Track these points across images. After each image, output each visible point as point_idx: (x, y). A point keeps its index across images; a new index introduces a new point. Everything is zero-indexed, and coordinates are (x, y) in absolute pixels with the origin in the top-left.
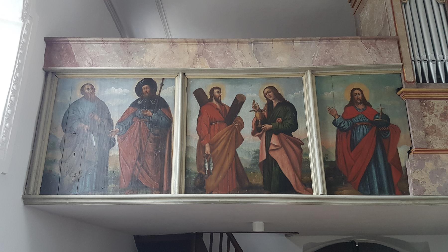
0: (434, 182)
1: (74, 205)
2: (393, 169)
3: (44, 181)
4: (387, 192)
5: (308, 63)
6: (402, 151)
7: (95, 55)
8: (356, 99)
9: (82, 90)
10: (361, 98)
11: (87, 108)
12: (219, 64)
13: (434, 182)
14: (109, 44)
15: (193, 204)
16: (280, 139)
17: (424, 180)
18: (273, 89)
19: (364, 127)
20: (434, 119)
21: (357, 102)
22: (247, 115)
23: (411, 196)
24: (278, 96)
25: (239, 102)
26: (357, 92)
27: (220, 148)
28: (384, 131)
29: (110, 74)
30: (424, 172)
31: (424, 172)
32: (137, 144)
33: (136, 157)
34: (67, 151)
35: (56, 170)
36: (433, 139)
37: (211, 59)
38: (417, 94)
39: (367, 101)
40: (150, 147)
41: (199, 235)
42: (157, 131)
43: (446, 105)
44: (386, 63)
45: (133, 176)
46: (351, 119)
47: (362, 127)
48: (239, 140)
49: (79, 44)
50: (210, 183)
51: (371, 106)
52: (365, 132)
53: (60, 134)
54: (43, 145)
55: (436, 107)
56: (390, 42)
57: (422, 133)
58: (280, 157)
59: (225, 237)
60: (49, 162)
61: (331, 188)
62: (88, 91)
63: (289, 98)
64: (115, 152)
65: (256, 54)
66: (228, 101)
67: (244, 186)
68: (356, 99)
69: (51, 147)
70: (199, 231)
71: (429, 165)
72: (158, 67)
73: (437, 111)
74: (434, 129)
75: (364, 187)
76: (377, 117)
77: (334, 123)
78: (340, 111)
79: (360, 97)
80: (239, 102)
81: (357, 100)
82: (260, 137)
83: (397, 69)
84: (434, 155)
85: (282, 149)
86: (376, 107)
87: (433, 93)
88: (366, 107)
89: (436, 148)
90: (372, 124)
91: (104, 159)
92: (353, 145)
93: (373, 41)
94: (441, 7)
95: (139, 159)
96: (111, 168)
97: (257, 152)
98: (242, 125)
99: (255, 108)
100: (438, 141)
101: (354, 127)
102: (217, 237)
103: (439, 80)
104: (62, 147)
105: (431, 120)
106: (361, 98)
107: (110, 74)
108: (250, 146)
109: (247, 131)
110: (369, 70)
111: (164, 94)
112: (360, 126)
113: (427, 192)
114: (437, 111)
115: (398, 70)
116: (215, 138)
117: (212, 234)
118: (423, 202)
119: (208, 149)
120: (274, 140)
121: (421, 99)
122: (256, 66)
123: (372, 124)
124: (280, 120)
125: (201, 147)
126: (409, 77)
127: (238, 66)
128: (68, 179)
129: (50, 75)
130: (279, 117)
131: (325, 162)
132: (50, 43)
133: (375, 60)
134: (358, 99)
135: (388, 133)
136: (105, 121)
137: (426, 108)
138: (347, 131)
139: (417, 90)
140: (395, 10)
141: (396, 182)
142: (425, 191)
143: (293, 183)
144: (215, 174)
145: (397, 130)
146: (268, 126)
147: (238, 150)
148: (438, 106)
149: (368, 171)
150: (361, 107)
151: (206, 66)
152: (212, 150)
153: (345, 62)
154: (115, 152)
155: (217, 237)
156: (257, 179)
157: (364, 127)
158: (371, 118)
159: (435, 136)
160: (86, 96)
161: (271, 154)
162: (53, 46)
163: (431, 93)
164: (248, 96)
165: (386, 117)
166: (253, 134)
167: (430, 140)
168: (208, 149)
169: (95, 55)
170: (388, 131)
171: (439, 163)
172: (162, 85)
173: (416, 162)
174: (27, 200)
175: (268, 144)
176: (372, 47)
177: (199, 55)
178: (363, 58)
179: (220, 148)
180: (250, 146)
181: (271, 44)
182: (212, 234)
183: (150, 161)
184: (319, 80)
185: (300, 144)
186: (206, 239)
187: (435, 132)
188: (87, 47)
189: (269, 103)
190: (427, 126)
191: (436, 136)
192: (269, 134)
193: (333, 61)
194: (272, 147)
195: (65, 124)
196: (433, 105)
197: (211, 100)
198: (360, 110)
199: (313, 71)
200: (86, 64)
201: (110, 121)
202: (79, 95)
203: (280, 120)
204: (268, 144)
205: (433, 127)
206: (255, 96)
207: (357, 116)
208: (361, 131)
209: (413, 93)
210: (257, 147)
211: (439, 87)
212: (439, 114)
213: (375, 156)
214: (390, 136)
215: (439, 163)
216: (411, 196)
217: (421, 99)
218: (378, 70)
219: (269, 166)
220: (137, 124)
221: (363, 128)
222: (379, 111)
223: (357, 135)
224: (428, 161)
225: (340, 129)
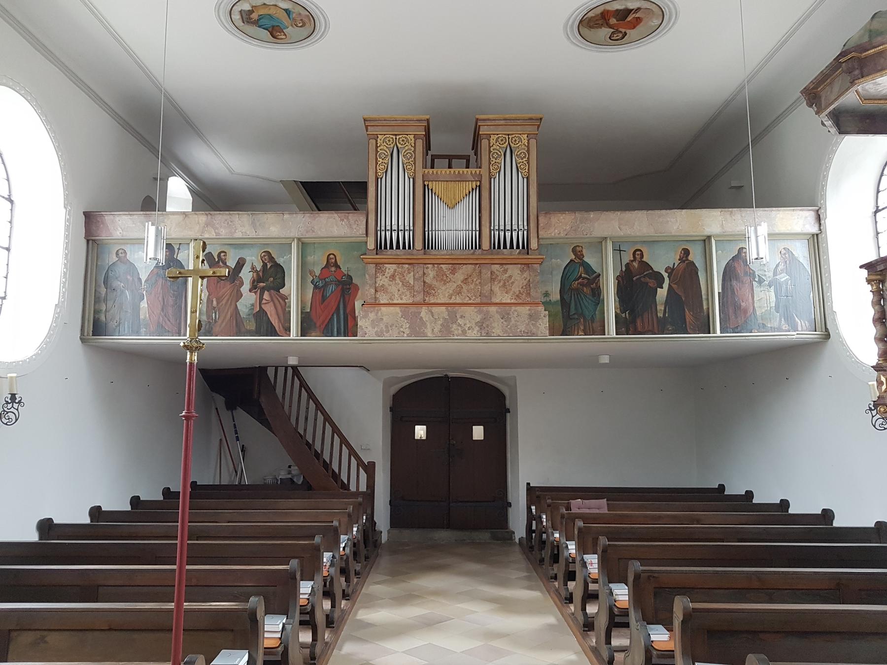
1: (119, 343)
2: (349, 317)
3: (95, 326)
5: (294, 233)
6: (358, 304)
7: (121, 225)
9: (117, 254)
11: (121, 269)
12: (223, 232)
14: (135, 217)
15: (229, 344)
16: (270, 295)
18: (268, 253)
22: (246, 275)
23: (291, 337)
24: (272, 259)
25: (240, 264)
26: (332, 256)
27: (224, 302)
28: (347, 288)
29: (142, 243)
32: (160, 299)
33: (160, 308)
34: (110, 304)
35: (103, 318)
37: (217, 228)
40: (171, 301)
41: (263, 370)
42: (176, 288)
45: (159, 322)
48: (240, 295)
49: (112, 217)
50: (216, 329)
53: (103, 290)
54: (91, 299)
58: (269, 309)
59: (290, 371)
60: (97, 312)
61: (304, 332)
62: (121, 255)
63: (280, 261)
64: (144, 304)
65: (253, 225)
66: (232, 263)
67: (240, 331)
69: (97, 300)
70: (263, 364)
71: (372, 316)
72: (173, 236)
75: (327, 331)
77: (312, 282)
78: (318, 273)
80: (240, 264)
81: (331, 263)
82: (255, 293)
85: (271, 303)
89: (382, 302)
90: (339, 283)
91: (136, 309)
92: (324, 298)
95: (163, 310)
96: (142, 317)
97: (253, 305)
98: (242, 284)
99: (253, 268)
101: (326, 285)
102: (281, 371)
104: (105, 300)
105: (382, 280)
107: (142, 243)
108: (248, 300)
109: (245, 288)
111: (181, 257)
116: (221, 293)
117: (276, 368)
119: (215, 303)
120: (266, 296)
121: (377, 264)
122: (253, 234)
123: (339, 283)
124: (272, 279)
125: (209, 301)
126: (371, 245)
127: (238, 234)
128: (112, 325)
129: (90, 242)
130: (271, 276)
131: (302, 313)
132: (88, 215)
136: (136, 280)
138: (320, 288)
141: (349, 327)
143: (277, 329)
144: (220, 322)
145: (357, 288)
146: (262, 284)
147: (238, 304)
149: (331, 319)
150: (333, 269)
151: (213, 235)
152: (218, 303)
153: (322, 233)
154: (144, 304)
155: (281, 371)
156: (252, 326)
158: (339, 279)
160: (120, 259)
161: (263, 306)
162: (91, 219)
164: (248, 259)
165: (350, 278)
166: (250, 291)
168: (215, 303)
169: (121, 225)
172: (179, 249)
174: (83, 340)
175: (261, 298)
177: (207, 225)
179: (224, 302)
180: (248, 300)
181: (266, 216)
182: (276, 368)
183: (170, 311)
184: (304, 245)
185: (285, 298)
186: (271, 372)
188: (117, 219)
189: (265, 265)
192: (263, 290)
193: (313, 231)
194: (264, 301)
195: (106, 282)
197: (218, 262)
199: (299, 239)
200: (118, 234)
201: (140, 280)
202: (115, 259)
203: (272, 279)
204: (261, 298)
205: (383, 286)
206: (254, 259)
208: (331, 288)
210: (253, 302)
212: (388, 276)
213: (338, 308)
216: (291, 337)
217: (377, 264)
219: (260, 316)
220: (160, 282)
225: (316, 287)
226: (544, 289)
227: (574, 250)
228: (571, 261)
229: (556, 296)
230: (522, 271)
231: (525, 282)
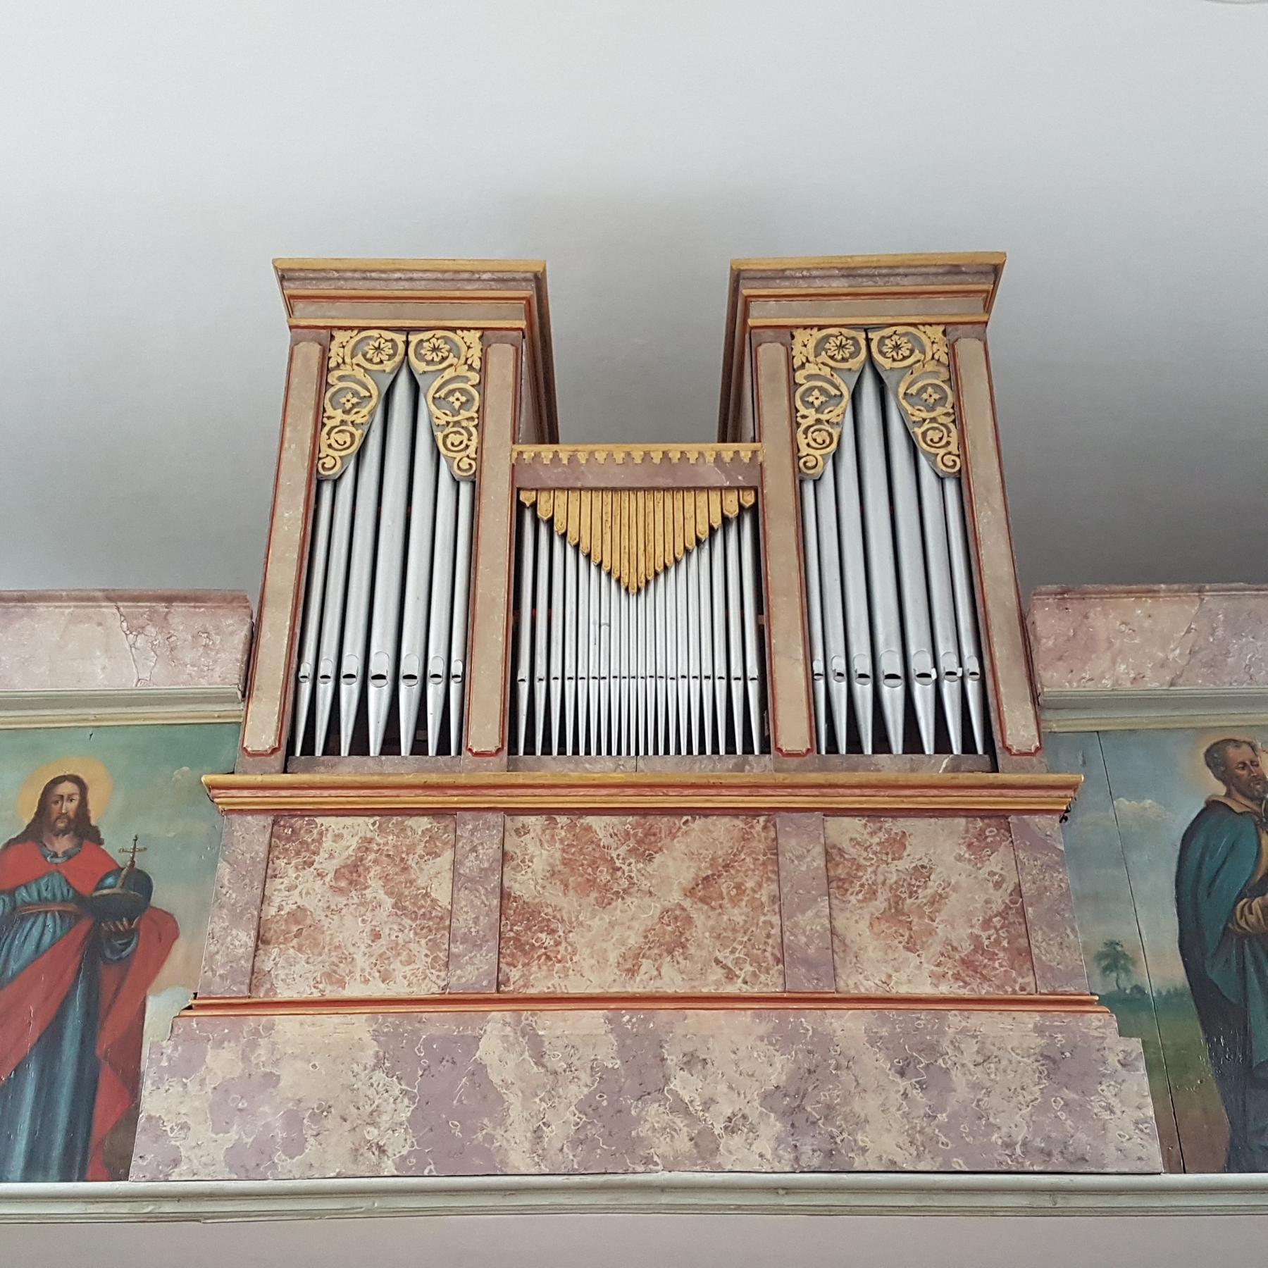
0: (221, 1126)
4: (54, 1170)
8: (55, 815)
10: (71, 814)
13: (221, 1126)
17: (184, 1119)
19: (49, 922)
20: (309, 885)
21: (52, 827)
26: (67, 788)
30: (193, 1088)
31: (193, 1088)
36: (281, 962)
38: (260, 793)
39: (93, 822)
43: (369, 835)
44: (183, 683)
46: (12, 893)
47: (41, 919)
51: (100, 842)
52: (47, 938)
55: (328, 843)
56: (221, 612)
57: (244, 938)
68: (55, 815)
73: (331, 856)
74: (297, 922)
76: (110, 881)
79: (70, 807)
83: (228, 707)
84: (252, 1022)
86: (115, 845)
87: (318, 792)
88: (80, 845)
93: (161, 607)
94: (951, 487)
100: (302, 966)
103: (942, 744)
105: (299, 888)
106: (71, 814)
110: (129, 710)
112: (37, 915)
113: (184, 1167)
114: (331, 856)
115: (233, 710)
118: (168, 1208)
121: (279, 815)
133: (146, 675)
134: (61, 816)
135: (128, 944)
137: (291, 846)
139: (1052, 778)
140: (280, 498)
142: (176, 1163)
145: (166, 930)
148: (338, 837)
157: (49, 922)
158: (86, 888)
159: (292, 951)
163: (313, 792)
165: (141, 883)
167: (268, 966)
170: (130, 933)
171: (262, 1053)
173: (175, 1048)
176: (151, 630)
178: (104, 668)
187: (299, 933)
190: (273, 911)
191: (300, 949)
196: (321, 834)
198: (56, 855)
205: (298, 915)
207: (37, 880)
209: (246, 793)
211: (463, 769)
212: (331, 867)
214: (134, 950)
215: (262, 1051)
218: (156, 709)
221: (45, 926)
222: (122, 860)
223: (14, 948)
224: (219, 1044)
226: (1100, 934)
227: (1216, 759)
228: (1212, 805)
229: (1162, 969)
230: (978, 845)
231: (1000, 899)
